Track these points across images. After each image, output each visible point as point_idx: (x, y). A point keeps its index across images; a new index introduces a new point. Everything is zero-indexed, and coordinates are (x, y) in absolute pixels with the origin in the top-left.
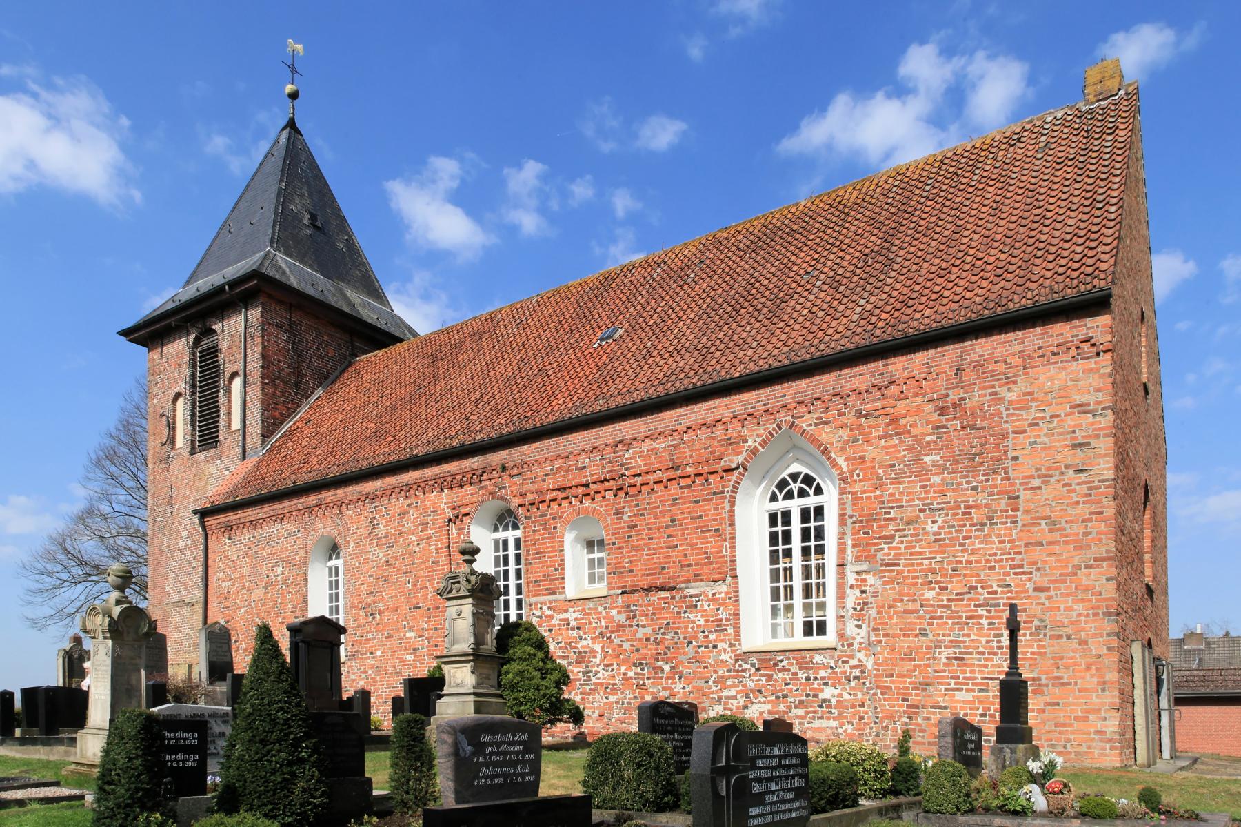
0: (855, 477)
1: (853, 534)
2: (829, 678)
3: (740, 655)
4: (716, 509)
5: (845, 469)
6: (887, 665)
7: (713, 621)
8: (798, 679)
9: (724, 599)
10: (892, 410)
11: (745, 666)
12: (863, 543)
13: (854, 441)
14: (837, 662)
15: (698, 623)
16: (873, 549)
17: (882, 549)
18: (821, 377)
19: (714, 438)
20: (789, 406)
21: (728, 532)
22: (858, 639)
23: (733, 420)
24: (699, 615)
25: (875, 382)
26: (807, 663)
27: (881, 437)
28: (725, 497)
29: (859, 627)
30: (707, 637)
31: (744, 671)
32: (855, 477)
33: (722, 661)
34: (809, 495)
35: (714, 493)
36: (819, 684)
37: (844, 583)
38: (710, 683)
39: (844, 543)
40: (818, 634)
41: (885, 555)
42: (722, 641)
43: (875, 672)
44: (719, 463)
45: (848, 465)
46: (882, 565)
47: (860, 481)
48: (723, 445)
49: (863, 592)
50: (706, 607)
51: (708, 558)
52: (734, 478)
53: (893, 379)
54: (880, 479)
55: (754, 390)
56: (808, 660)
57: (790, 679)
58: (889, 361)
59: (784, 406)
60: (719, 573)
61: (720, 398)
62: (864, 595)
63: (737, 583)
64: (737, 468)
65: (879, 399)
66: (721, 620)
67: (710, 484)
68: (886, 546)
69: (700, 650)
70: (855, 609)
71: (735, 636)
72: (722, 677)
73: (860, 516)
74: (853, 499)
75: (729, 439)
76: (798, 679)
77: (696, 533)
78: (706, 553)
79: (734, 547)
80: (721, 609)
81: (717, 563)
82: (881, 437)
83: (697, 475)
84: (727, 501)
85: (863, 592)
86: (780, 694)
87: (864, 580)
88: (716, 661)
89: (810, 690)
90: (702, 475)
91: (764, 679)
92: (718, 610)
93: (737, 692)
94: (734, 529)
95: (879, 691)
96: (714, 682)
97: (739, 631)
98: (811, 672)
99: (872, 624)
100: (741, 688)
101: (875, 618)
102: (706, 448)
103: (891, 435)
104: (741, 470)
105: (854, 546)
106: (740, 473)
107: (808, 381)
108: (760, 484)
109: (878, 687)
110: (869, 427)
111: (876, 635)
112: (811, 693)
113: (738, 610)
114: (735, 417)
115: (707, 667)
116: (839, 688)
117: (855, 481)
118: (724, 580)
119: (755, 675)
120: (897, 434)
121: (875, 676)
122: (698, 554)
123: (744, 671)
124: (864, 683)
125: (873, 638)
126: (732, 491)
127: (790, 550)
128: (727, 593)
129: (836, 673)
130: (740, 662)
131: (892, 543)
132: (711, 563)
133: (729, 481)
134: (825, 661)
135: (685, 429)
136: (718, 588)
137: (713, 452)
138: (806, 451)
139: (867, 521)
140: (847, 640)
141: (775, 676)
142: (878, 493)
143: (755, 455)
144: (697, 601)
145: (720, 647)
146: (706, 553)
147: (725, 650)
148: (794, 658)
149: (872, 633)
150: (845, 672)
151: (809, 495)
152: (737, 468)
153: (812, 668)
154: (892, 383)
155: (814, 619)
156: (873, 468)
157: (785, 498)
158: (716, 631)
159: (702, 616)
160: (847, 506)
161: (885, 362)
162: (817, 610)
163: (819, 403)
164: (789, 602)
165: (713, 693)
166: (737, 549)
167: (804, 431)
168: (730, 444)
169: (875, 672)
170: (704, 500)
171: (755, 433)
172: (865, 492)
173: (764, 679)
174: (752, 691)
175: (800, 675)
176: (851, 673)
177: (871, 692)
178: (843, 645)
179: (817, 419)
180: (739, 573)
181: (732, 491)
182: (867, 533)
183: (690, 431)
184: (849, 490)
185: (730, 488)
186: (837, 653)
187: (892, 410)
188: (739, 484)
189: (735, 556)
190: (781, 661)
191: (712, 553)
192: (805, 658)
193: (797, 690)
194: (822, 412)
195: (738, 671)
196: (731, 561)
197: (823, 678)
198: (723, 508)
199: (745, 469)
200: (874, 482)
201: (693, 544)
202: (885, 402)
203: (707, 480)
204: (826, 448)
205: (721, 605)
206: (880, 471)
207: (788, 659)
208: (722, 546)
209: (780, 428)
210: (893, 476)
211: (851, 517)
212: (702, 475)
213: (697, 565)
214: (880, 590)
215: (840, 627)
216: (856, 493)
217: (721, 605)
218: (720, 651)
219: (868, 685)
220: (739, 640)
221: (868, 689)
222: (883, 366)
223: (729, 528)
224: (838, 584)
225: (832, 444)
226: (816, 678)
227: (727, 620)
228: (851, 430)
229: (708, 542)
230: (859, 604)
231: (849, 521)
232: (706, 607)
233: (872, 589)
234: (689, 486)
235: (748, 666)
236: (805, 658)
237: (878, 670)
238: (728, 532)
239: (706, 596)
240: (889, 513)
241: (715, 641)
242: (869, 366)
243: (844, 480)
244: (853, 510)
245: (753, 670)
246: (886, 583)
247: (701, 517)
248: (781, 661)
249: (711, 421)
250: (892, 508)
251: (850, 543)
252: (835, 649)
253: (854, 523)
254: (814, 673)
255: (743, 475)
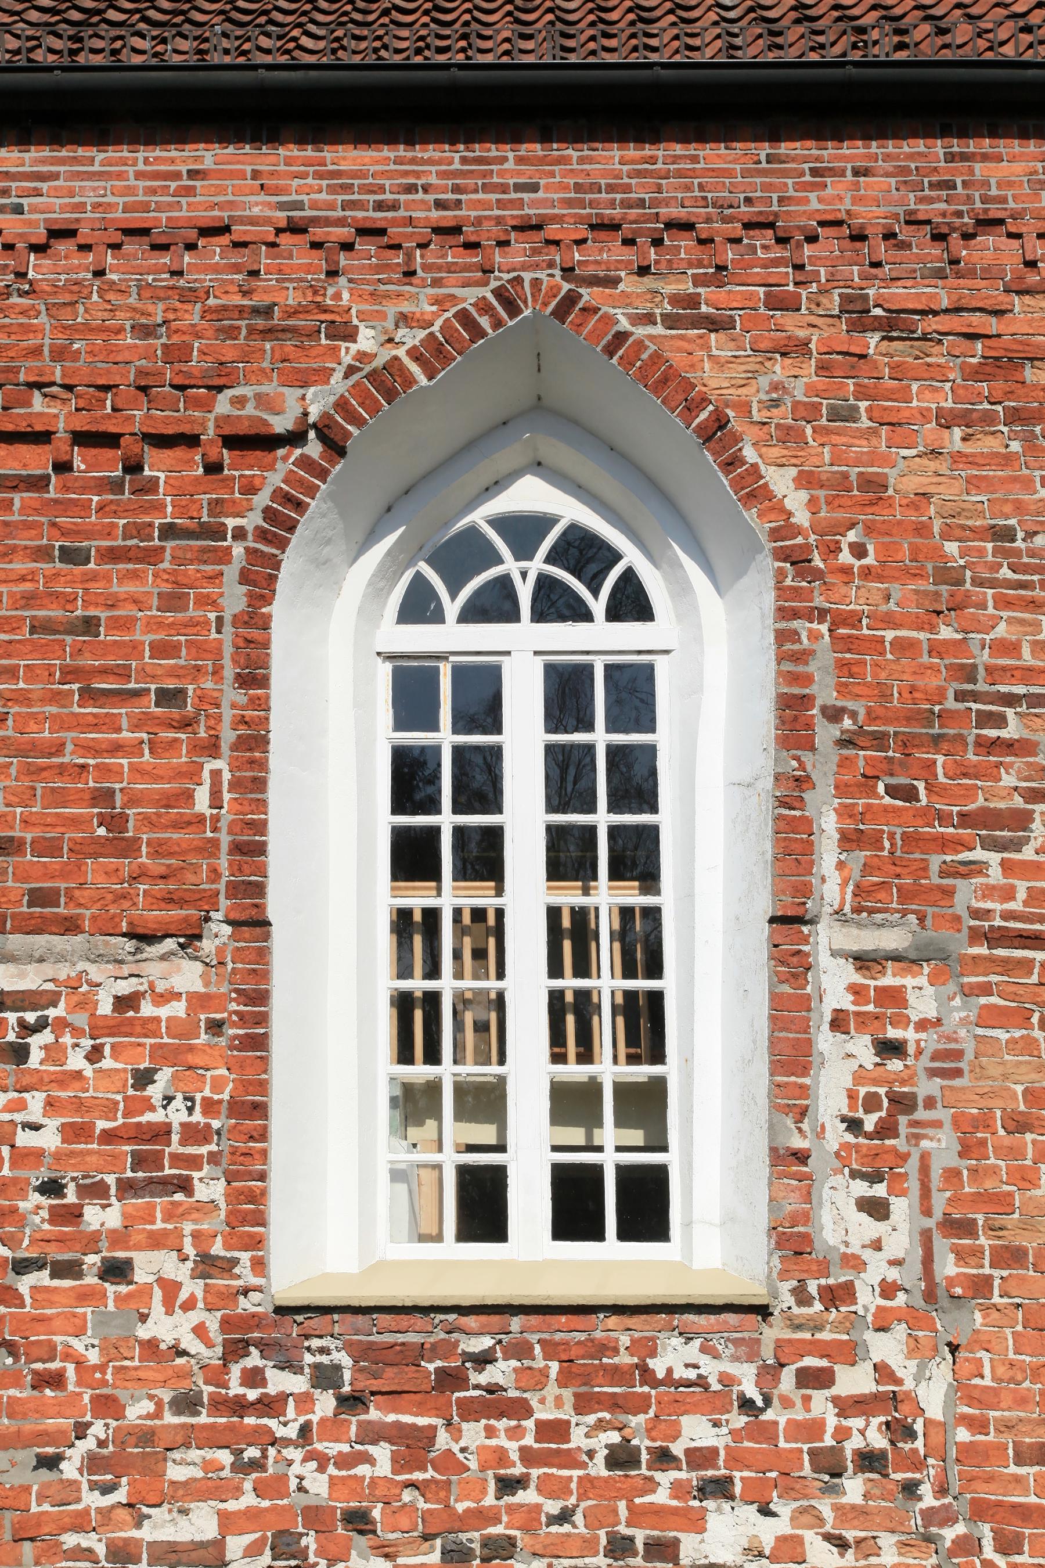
0: (845, 557)
1: (841, 789)
2: (735, 1459)
3: (254, 1321)
4: (172, 601)
5: (802, 518)
6: (1022, 1401)
7: (108, 1137)
8: (569, 1460)
9: (182, 1029)
10: (993, 325)
11: (279, 1381)
12: (892, 831)
13: (835, 415)
14: (769, 1374)
15: (24, 1139)
16: (935, 861)
17: (977, 868)
18: (692, 149)
19: (189, 296)
20: (552, 231)
21: (228, 714)
22: (877, 1270)
23: (285, 239)
24: (36, 1101)
25: (924, 211)
26: (617, 1375)
27: (946, 420)
28: (225, 557)
29: (877, 1209)
30: (74, 1214)
31: (271, 1406)
32: (845, 557)
33: (151, 1346)
34: (587, 616)
35: (169, 531)
36: (678, 1489)
37: (805, 1003)
38: (69, 1469)
39: (806, 825)
40: (625, 1234)
41: (989, 892)
42: (157, 1242)
43: (963, 1435)
44: (207, 406)
45: (812, 504)
46: (976, 936)
47: (867, 573)
48: (232, 333)
49: (889, 1049)
50: (76, 1061)
51: (115, 822)
52: (275, 479)
53: (995, 211)
54: (950, 576)
55: (391, 140)
56: (625, 1359)
57: (528, 1456)
58: (972, 146)
59: (526, 227)
60: (170, 900)
61: (224, 140)
62: (895, 1065)
63: (263, 955)
64: (295, 438)
65: (940, 274)
66: (161, 1133)
67: (152, 486)
68: (994, 858)
69: (25, 1284)
70: (854, 1125)
71: (236, 1219)
72: (146, 1436)
73: (872, 716)
74: (841, 643)
75: (267, 311)
76: (569, 1460)
77: (57, 697)
78: (104, 797)
79: (260, 784)
80: (164, 1076)
81: (158, 850)
82: (946, 420)
83: (82, 438)
84: (231, 572)
85: (889, 1049)
86: (473, 1538)
87: (894, 997)
88: (112, 1349)
89: (637, 1516)
90: (111, 440)
91: (383, 1453)
92: (144, 1079)
93: (227, 1522)
94: (262, 704)
95: (986, 1531)
96: (93, 1463)
97: (258, 1197)
98: (638, 1420)
99: (939, 1202)
100: (248, 1500)
101: (952, 1175)
102: (146, 331)
103: (989, 418)
104: (314, 448)
105: (849, 840)
106: (305, 462)
107: (632, 151)
108: (371, 537)
109: (980, 1511)
110: (899, 373)
111: (961, 1256)
112: (640, 1536)
113: (263, 1087)
114: (295, 228)
115: (56, 1380)
116: (785, 1509)
117: (846, 570)
118: (192, 938)
119: (332, 1428)
120: (1014, 417)
121: (966, 1451)
122: (58, 797)
123: (271, 1406)
124: (910, 1489)
125: (948, 1267)
126: (262, 535)
127: (494, 837)
128: (198, 1001)
129: (768, 1433)
130: (254, 1359)
131: (1017, 845)
132: (130, 848)
133: (250, 489)
134: (711, 1369)
135: (40, 235)
136: (154, 970)
137: (176, 354)
138: (575, 422)
139: (906, 744)
140: (823, 1268)
141: (443, 1440)
142: (946, 633)
143: (390, 395)
144: (27, 1029)
145: (141, 1276)
146: (104, 797)
147: (170, 1288)
148: (551, 1349)
149: (941, 1245)
150: (815, 1428)
151: (587, 616)
152: (295, 438)
153: (641, 1405)
154: (988, 223)
155: (609, 1161)
156: (922, 530)
157: (473, 613)
158: (127, 1188)
159: (51, 1105)
160: (812, 667)
161: (956, 146)
162: (460, 1115)
163: (685, 243)
164: (643, 1072)
165: (80, 1523)
166: (274, 794)
167: (621, 337)
168: (268, 333)
169: (963, 1435)
170: (112, 555)
171: (391, 310)
172: (889, 621)
173: (383, 1453)
174: (315, 1516)
175: (578, 1439)
176: (842, 1434)
177: (949, 1534)
178: (802, 1297)
179: (676, 300)
180: (275, 908)
181: (262, 535)
182: (909, 794)
183: (62, 247)
184: (819, 601)
185: (252, 520)
186: (772, 1333)
187: (993, 325)
188: (300, 506)
189: (261, 827)
190: (483, 1360)
191: (133, 801)
192: (610, 1348)
193: (564, 1517)
194: (697, 281)
195: (240, 1407)
196: (237, 848)
197: (701, 1457)
198: (209, 602)
199: (336, 448)
200: (927, 586)
201: (34, 749)
202: (966, 290)
203: (134, 467)
204: (720, 422)
205: (163, 1055)
206: (952, 548)
207: (520, 1350)
208: (193, 773)
209: (513, 309)
210: (1005, 573)
211: (834, 715)
212: (111, 440)
213: (49, 848)
214: (969, 1048)
215: (792, 1205)
216: (853, 619)
217: (163, 1055)
218: (146, 1291)
219: (929, 1500)
220: (257, 1243)
221: (929, 1515)
222: (950, 158)
223: (232, 695)
224: (777, 1002)
225: (744, 408)
226: (663, 1458)
227: (193, 1134)
228: (823, 368)
229: (116, 749)
230: (871, 1103)
231: (826, 733)
232: (76, 1061)
233: (930, 1040)
234: (39, 483)
235: (297, 1383)
236: (610, 1348)
237: (979, 1425)
238: (228, 714)
239: (86, 1004)
240: (1000, 721)
241: (118, 1238)
242: (891, 146)
243: (798, 560)
244: (842, 689)
245: (325, 1404)
246: (990, 1017)
247: (89, 625)
248: (483, 1360)
249: (174, 225)
250: (1011, 700)
251: (829, 824)
252: (763, 1311)
253: (846, 742)
254: (650, 1431)
255: (323, 474)
